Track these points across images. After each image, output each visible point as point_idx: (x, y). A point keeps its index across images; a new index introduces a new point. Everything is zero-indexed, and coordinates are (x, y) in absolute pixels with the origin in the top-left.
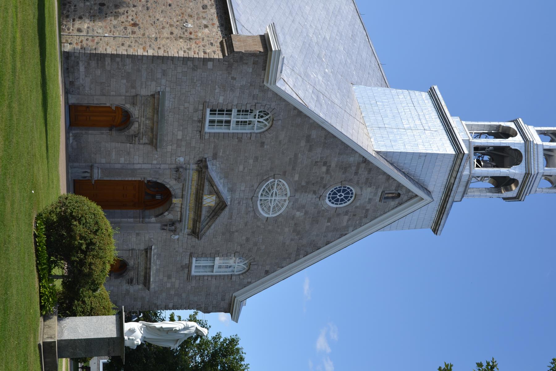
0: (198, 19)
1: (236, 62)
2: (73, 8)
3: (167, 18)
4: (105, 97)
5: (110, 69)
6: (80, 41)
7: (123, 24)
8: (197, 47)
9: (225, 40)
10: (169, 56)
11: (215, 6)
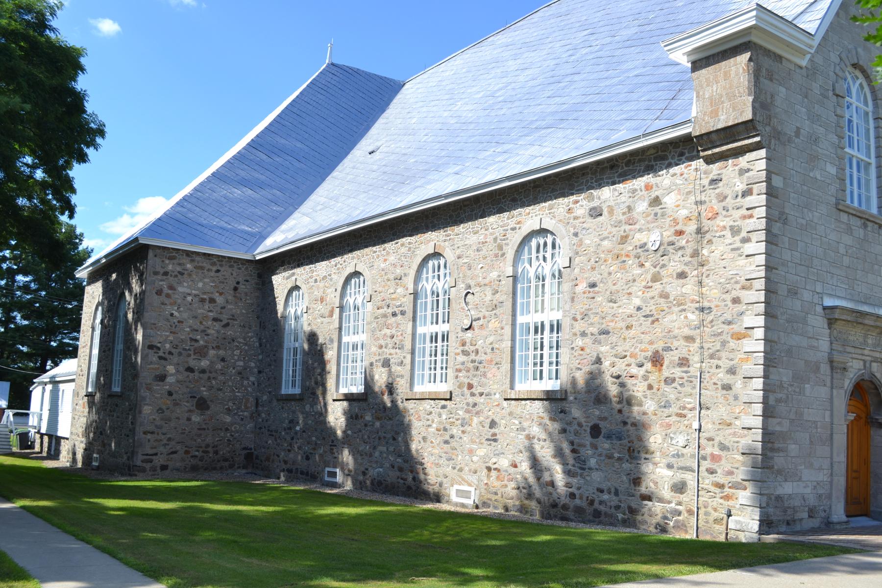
0: (631, 222)
1: (770, 120)
2: (605, 497)
3: (633, 289)
4: (835, 436)
5: (788, 421)
6: (718, 490)
7: (656, 386)
8: (729, 213)
9: (703, 151)
10: (764, 276)
11: (592, 191)
